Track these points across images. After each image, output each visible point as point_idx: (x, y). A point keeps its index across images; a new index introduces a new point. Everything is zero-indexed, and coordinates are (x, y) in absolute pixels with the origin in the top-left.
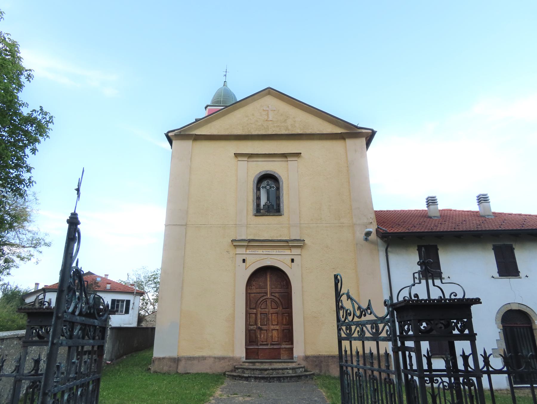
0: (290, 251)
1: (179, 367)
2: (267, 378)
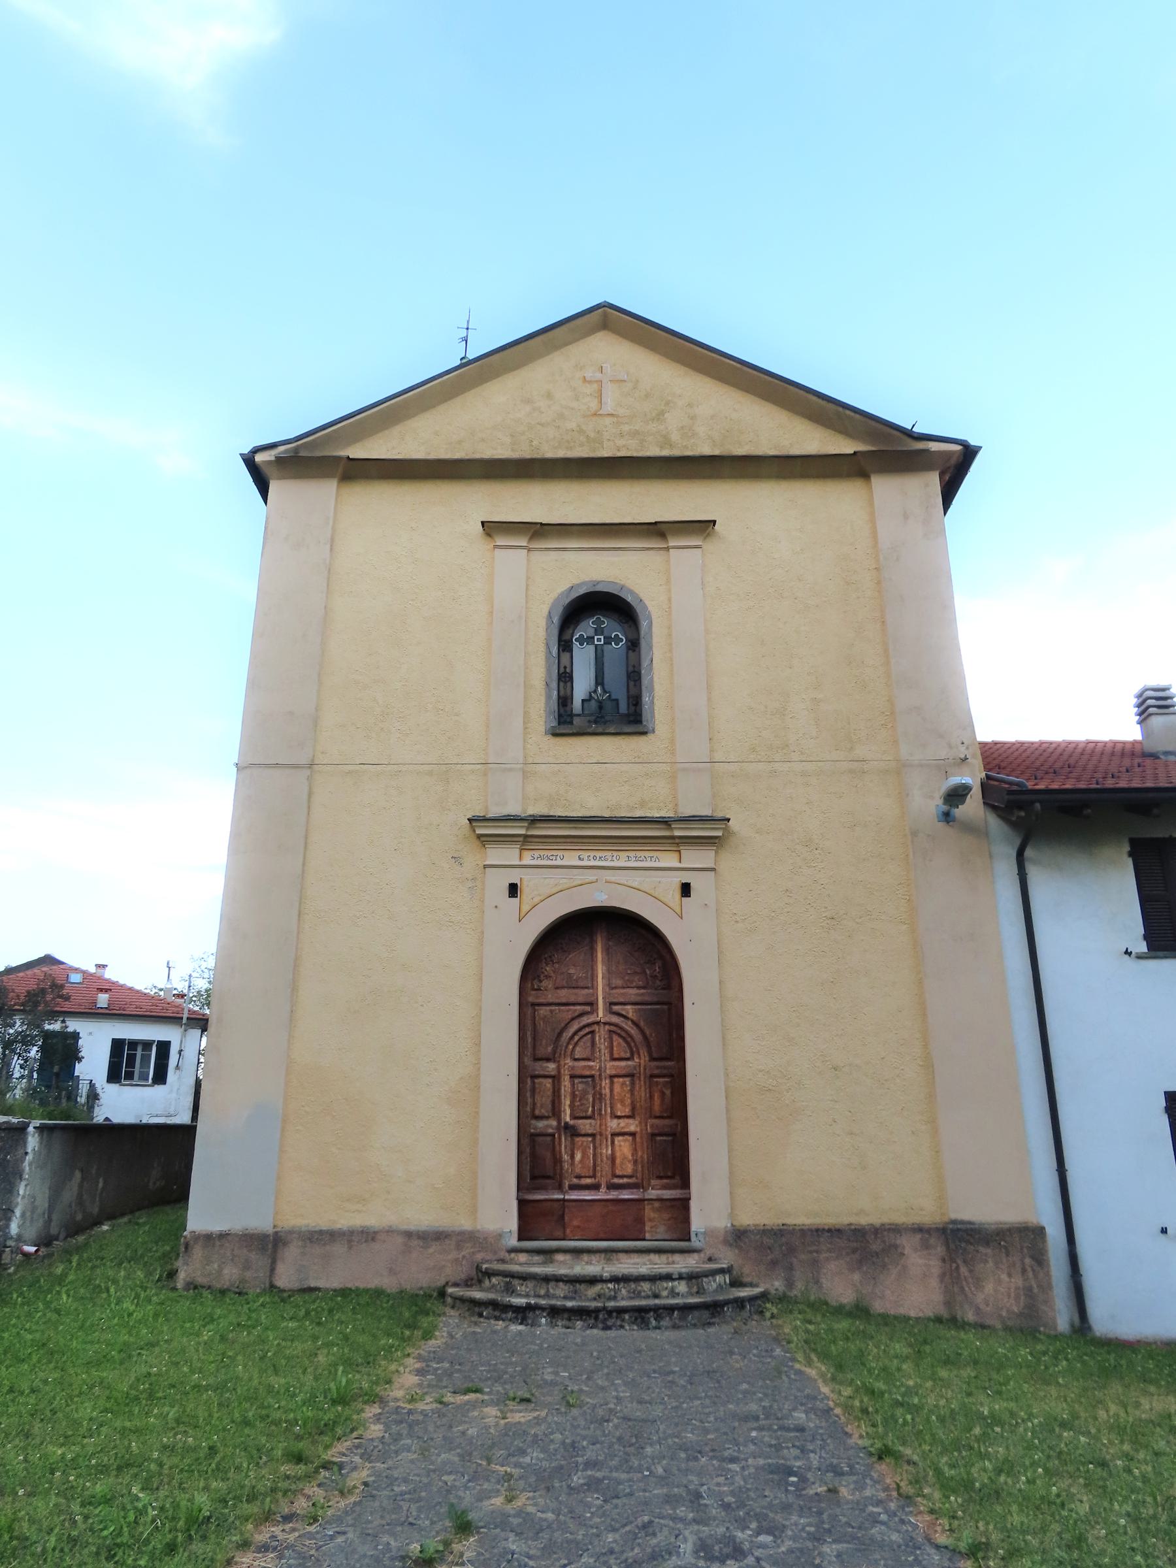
0: (676, 855)
1: (280, 1268)
2: (597, 1311)
